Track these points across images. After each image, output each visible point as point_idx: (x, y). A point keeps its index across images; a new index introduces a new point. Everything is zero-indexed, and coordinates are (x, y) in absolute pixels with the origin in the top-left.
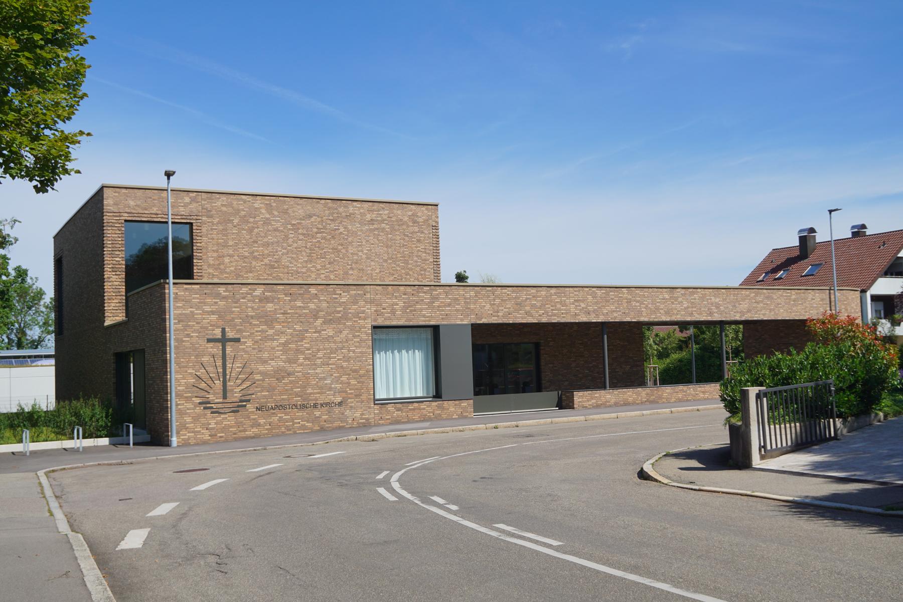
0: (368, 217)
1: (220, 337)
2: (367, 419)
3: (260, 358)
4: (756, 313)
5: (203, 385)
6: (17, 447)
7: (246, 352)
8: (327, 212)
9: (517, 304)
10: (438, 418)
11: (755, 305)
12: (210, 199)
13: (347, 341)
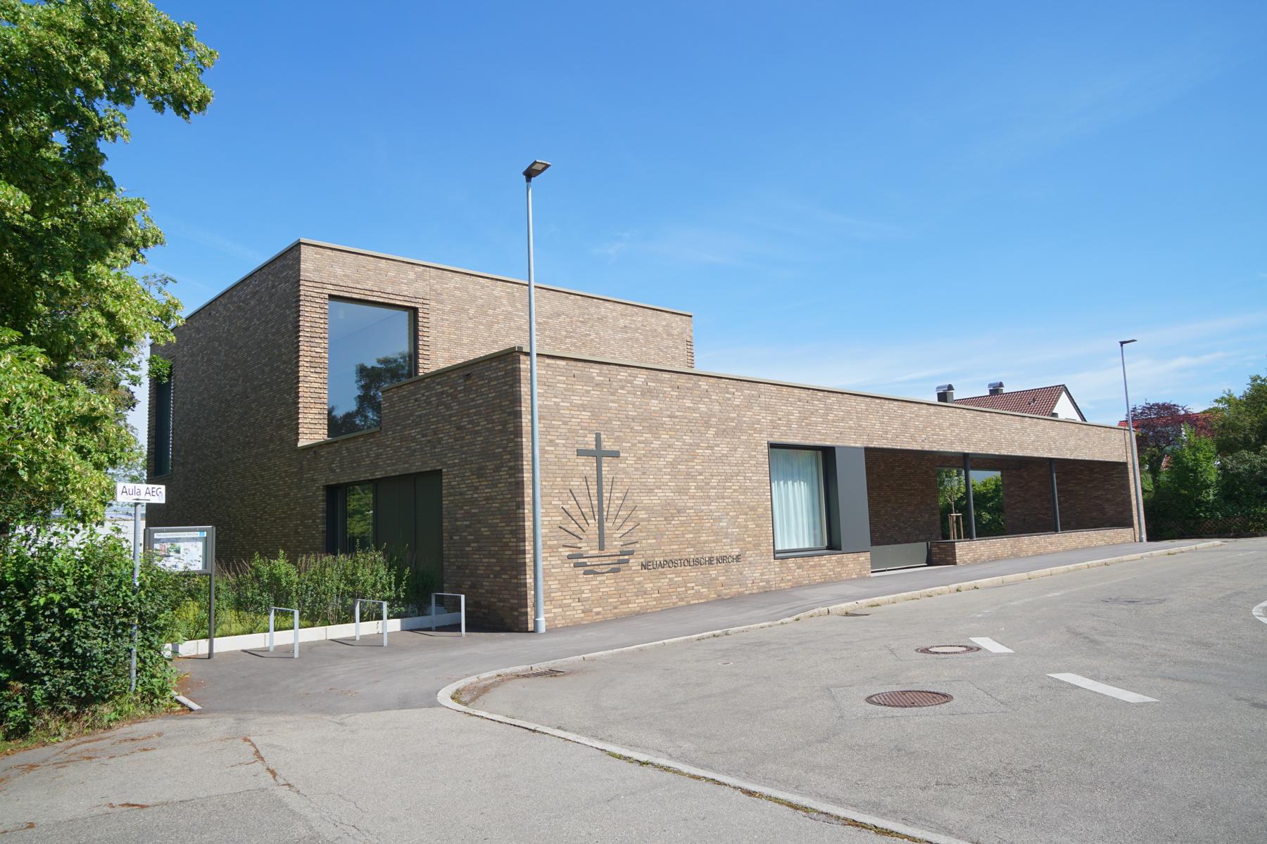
0: (622, 322)
1: (593, 447)
2: (768, 581)
5: (573, 527)
6: (283, 638)
7: (626, 473)
8: (577, 311)
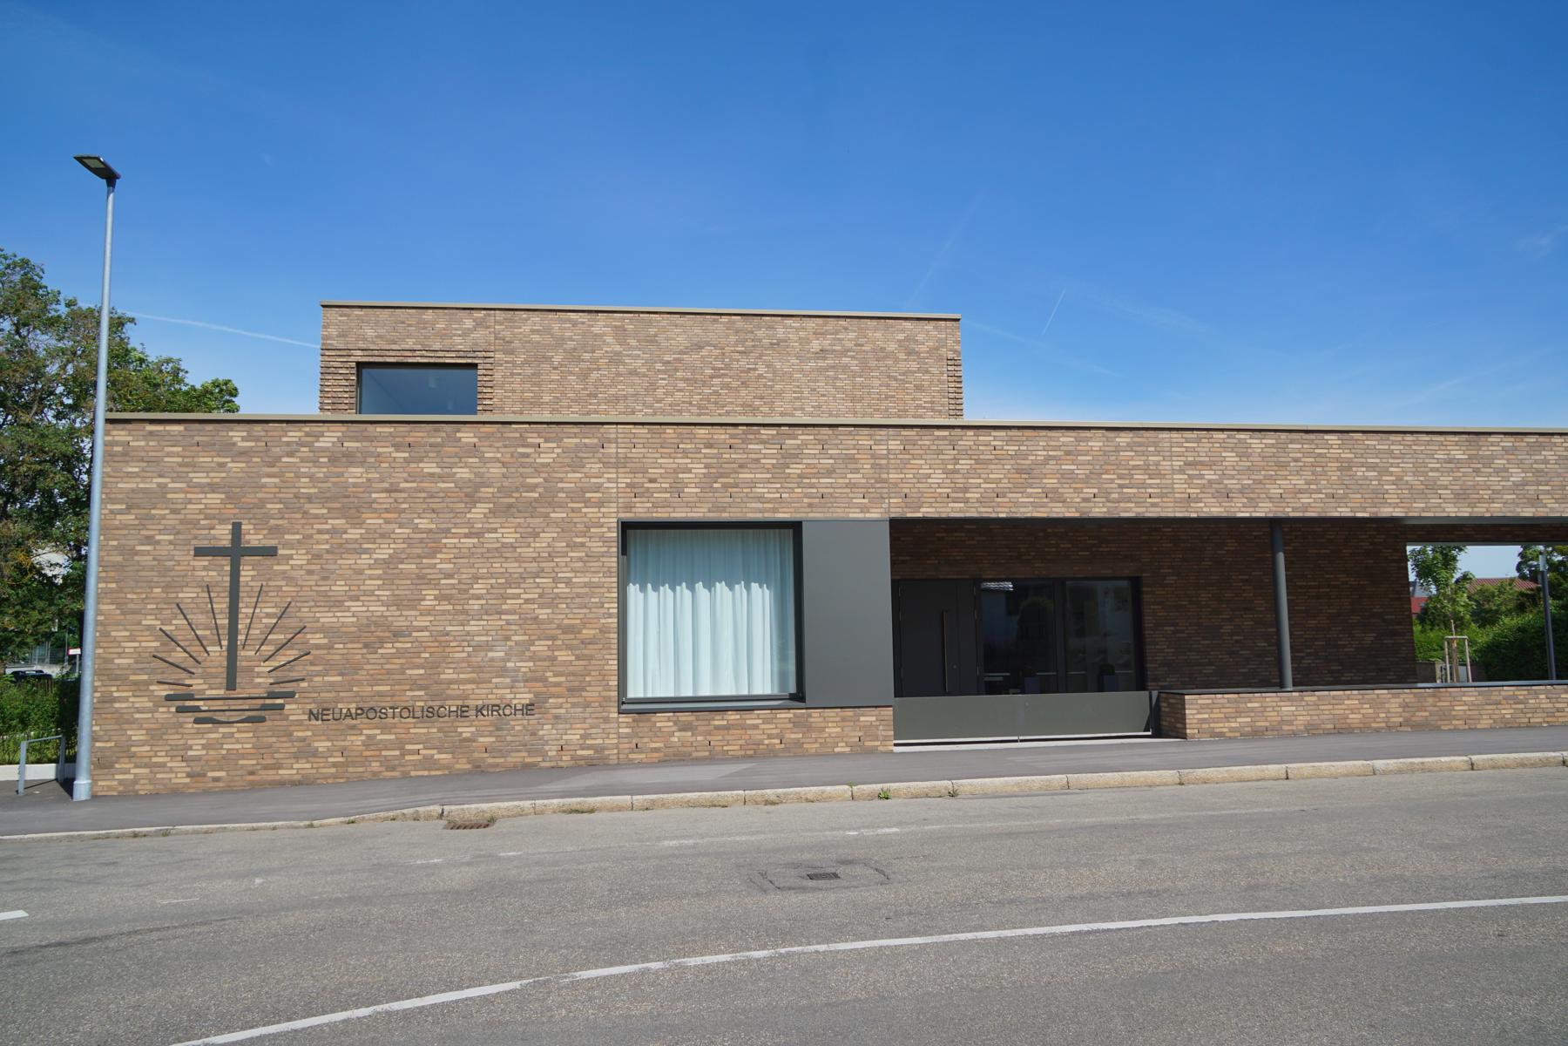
0: (816, 345)
2: (599, 749)
3: (325, 595)
5: (178, 656)
8: (733, 339)
9: (1019, 471)
10: (794, 751)
12: (510, 320)
13: (551, 557)
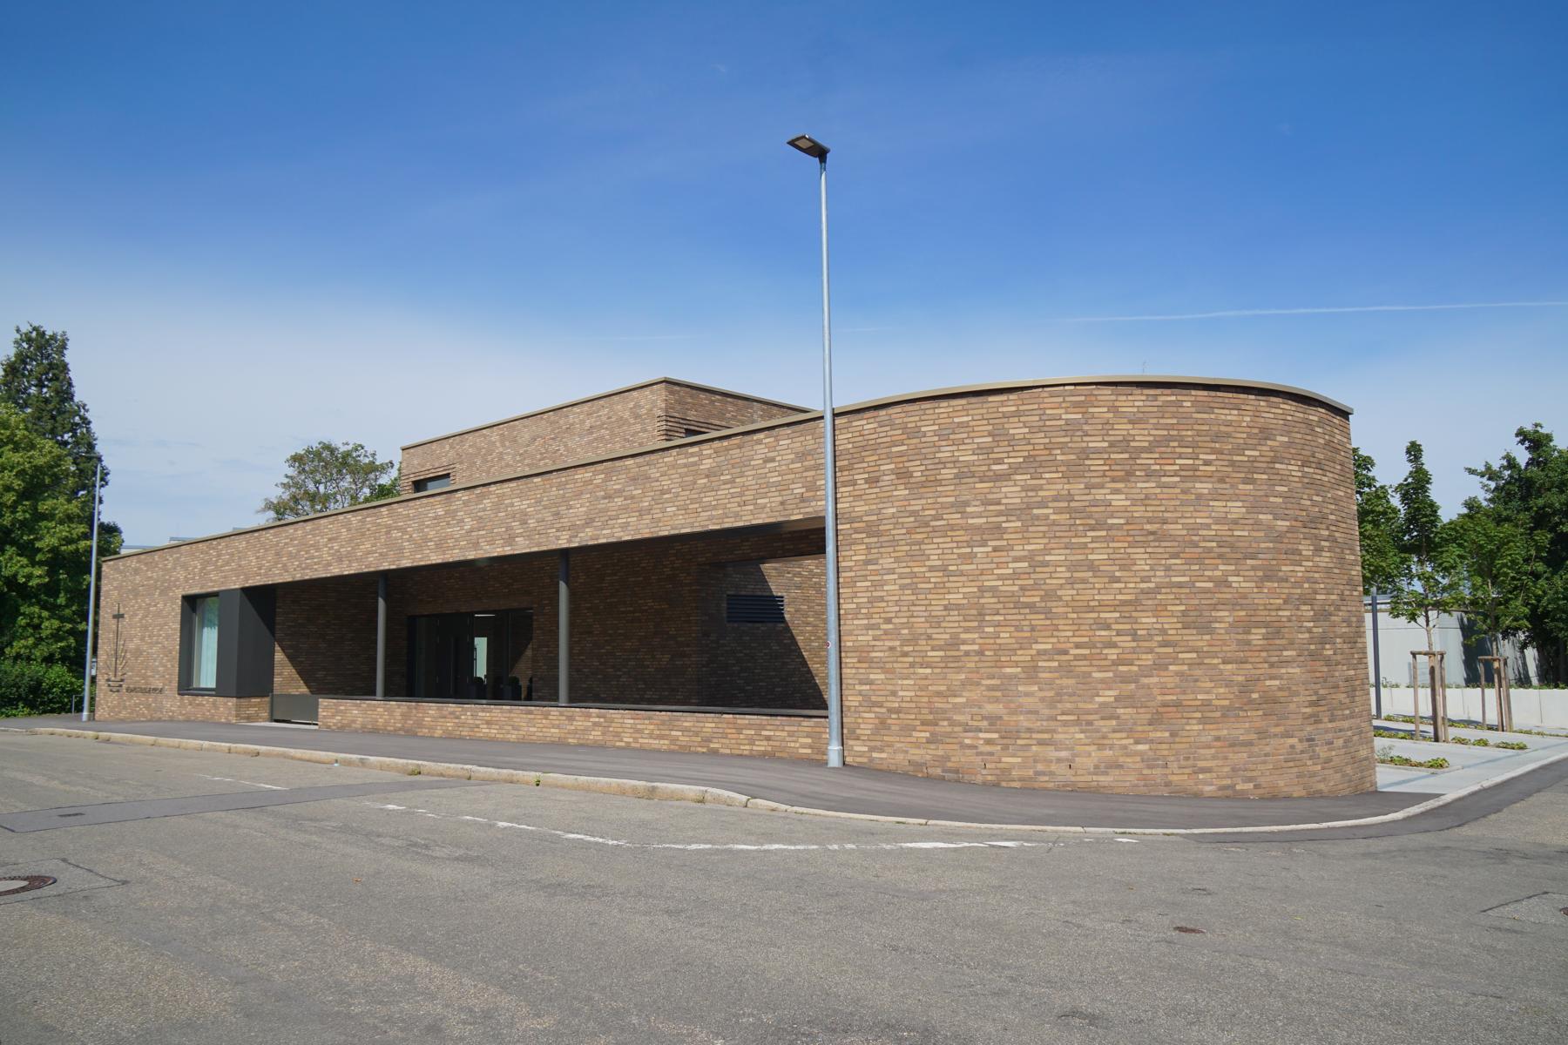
4: (605, 525)
11: (604, 504)
